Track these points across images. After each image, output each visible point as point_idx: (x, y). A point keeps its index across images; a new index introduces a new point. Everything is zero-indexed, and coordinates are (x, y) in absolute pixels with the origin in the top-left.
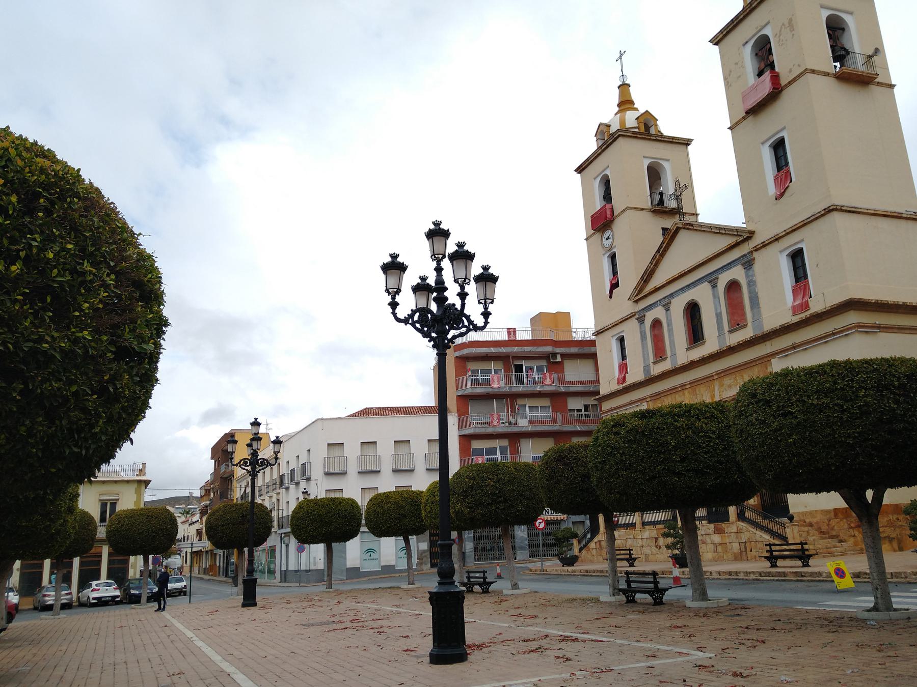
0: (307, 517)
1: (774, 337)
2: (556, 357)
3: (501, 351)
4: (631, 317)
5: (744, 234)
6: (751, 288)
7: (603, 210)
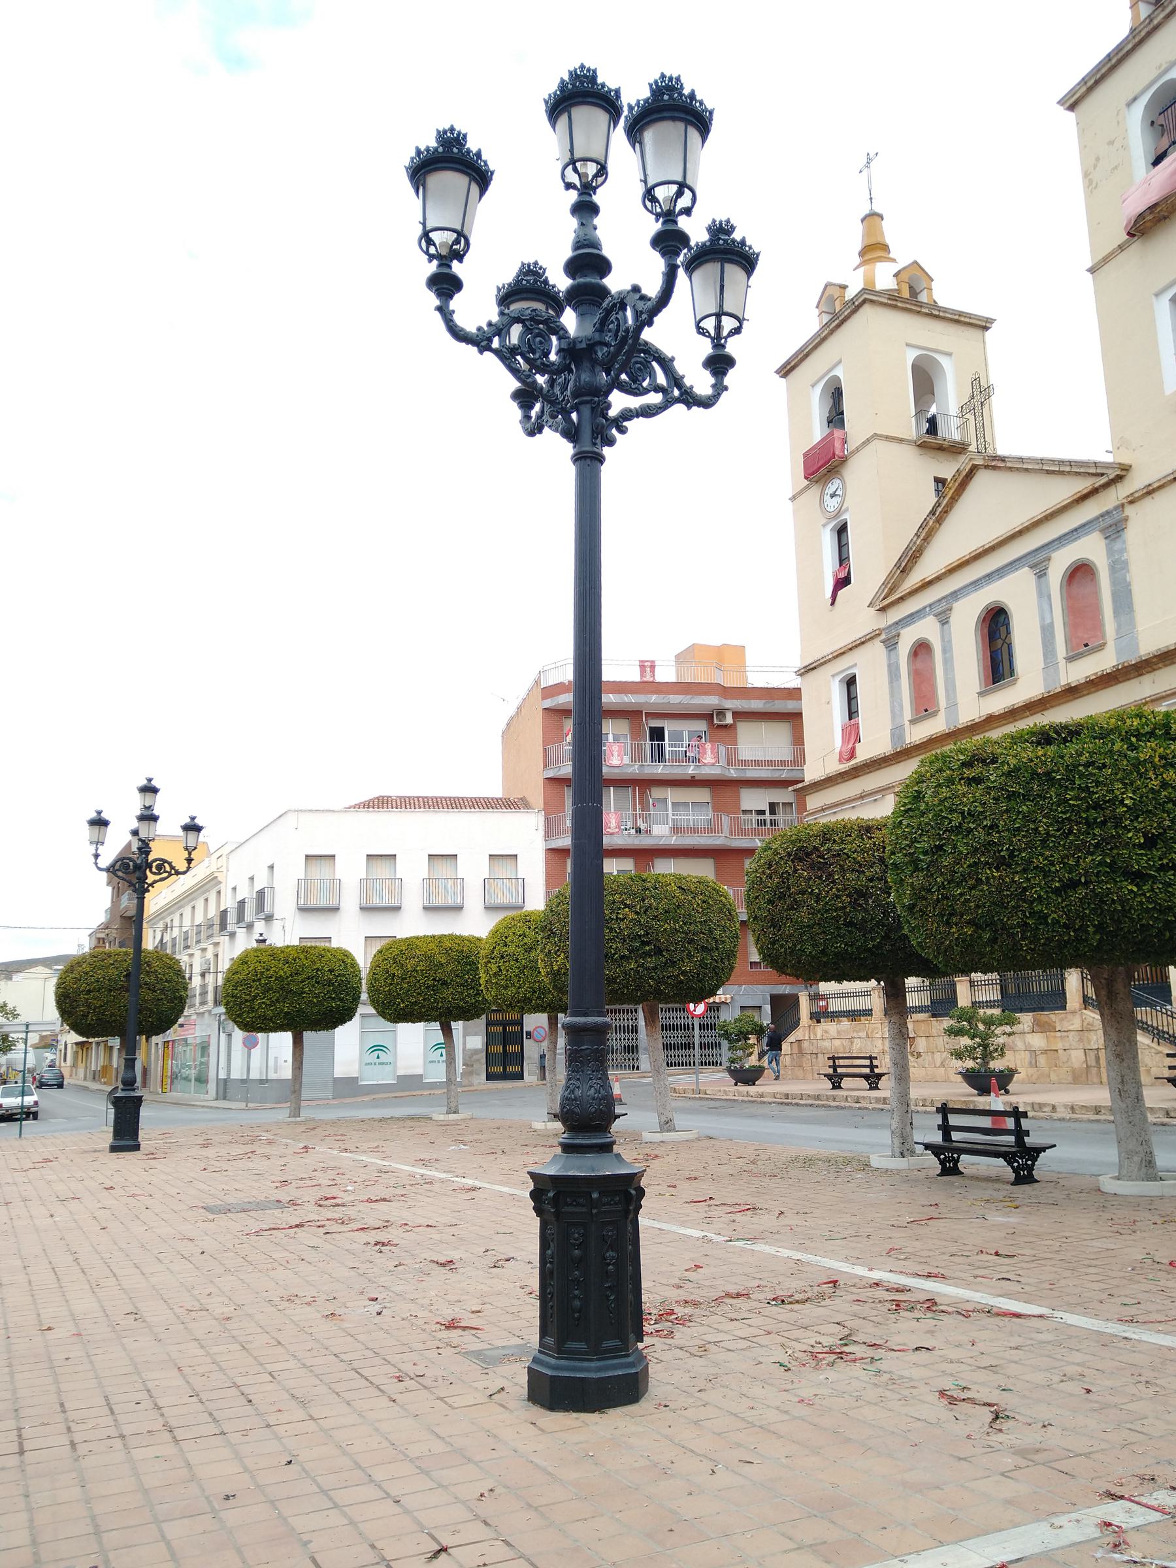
0: (254, 981)
1: (1160, 665)
2: (724, 715)
3: (626, 700)
4: (871, 639)
5: (1109, 471)
6: (1116, 575)
7: (825, 446)
